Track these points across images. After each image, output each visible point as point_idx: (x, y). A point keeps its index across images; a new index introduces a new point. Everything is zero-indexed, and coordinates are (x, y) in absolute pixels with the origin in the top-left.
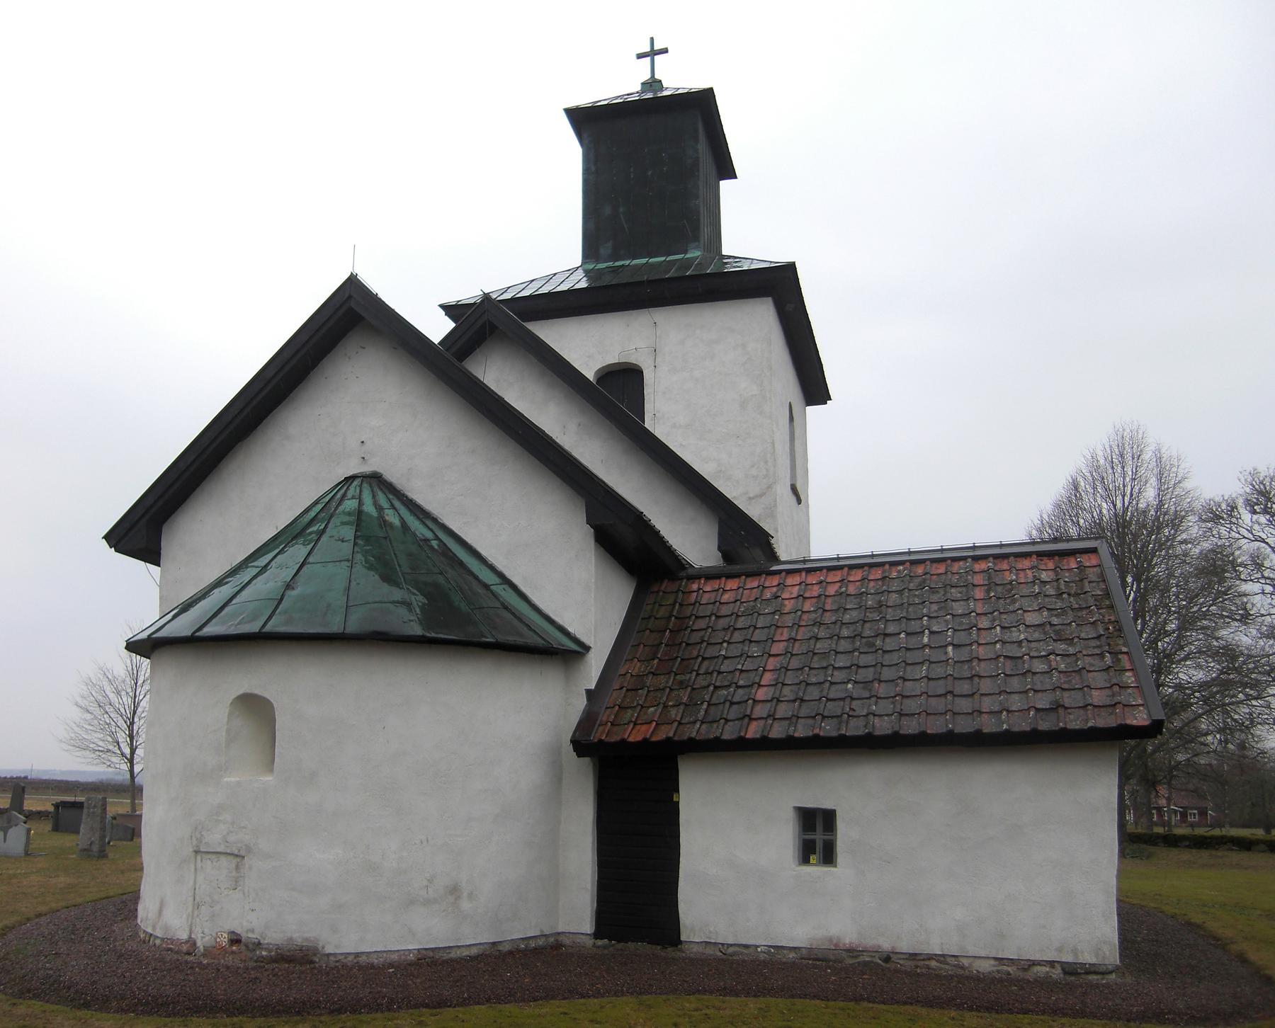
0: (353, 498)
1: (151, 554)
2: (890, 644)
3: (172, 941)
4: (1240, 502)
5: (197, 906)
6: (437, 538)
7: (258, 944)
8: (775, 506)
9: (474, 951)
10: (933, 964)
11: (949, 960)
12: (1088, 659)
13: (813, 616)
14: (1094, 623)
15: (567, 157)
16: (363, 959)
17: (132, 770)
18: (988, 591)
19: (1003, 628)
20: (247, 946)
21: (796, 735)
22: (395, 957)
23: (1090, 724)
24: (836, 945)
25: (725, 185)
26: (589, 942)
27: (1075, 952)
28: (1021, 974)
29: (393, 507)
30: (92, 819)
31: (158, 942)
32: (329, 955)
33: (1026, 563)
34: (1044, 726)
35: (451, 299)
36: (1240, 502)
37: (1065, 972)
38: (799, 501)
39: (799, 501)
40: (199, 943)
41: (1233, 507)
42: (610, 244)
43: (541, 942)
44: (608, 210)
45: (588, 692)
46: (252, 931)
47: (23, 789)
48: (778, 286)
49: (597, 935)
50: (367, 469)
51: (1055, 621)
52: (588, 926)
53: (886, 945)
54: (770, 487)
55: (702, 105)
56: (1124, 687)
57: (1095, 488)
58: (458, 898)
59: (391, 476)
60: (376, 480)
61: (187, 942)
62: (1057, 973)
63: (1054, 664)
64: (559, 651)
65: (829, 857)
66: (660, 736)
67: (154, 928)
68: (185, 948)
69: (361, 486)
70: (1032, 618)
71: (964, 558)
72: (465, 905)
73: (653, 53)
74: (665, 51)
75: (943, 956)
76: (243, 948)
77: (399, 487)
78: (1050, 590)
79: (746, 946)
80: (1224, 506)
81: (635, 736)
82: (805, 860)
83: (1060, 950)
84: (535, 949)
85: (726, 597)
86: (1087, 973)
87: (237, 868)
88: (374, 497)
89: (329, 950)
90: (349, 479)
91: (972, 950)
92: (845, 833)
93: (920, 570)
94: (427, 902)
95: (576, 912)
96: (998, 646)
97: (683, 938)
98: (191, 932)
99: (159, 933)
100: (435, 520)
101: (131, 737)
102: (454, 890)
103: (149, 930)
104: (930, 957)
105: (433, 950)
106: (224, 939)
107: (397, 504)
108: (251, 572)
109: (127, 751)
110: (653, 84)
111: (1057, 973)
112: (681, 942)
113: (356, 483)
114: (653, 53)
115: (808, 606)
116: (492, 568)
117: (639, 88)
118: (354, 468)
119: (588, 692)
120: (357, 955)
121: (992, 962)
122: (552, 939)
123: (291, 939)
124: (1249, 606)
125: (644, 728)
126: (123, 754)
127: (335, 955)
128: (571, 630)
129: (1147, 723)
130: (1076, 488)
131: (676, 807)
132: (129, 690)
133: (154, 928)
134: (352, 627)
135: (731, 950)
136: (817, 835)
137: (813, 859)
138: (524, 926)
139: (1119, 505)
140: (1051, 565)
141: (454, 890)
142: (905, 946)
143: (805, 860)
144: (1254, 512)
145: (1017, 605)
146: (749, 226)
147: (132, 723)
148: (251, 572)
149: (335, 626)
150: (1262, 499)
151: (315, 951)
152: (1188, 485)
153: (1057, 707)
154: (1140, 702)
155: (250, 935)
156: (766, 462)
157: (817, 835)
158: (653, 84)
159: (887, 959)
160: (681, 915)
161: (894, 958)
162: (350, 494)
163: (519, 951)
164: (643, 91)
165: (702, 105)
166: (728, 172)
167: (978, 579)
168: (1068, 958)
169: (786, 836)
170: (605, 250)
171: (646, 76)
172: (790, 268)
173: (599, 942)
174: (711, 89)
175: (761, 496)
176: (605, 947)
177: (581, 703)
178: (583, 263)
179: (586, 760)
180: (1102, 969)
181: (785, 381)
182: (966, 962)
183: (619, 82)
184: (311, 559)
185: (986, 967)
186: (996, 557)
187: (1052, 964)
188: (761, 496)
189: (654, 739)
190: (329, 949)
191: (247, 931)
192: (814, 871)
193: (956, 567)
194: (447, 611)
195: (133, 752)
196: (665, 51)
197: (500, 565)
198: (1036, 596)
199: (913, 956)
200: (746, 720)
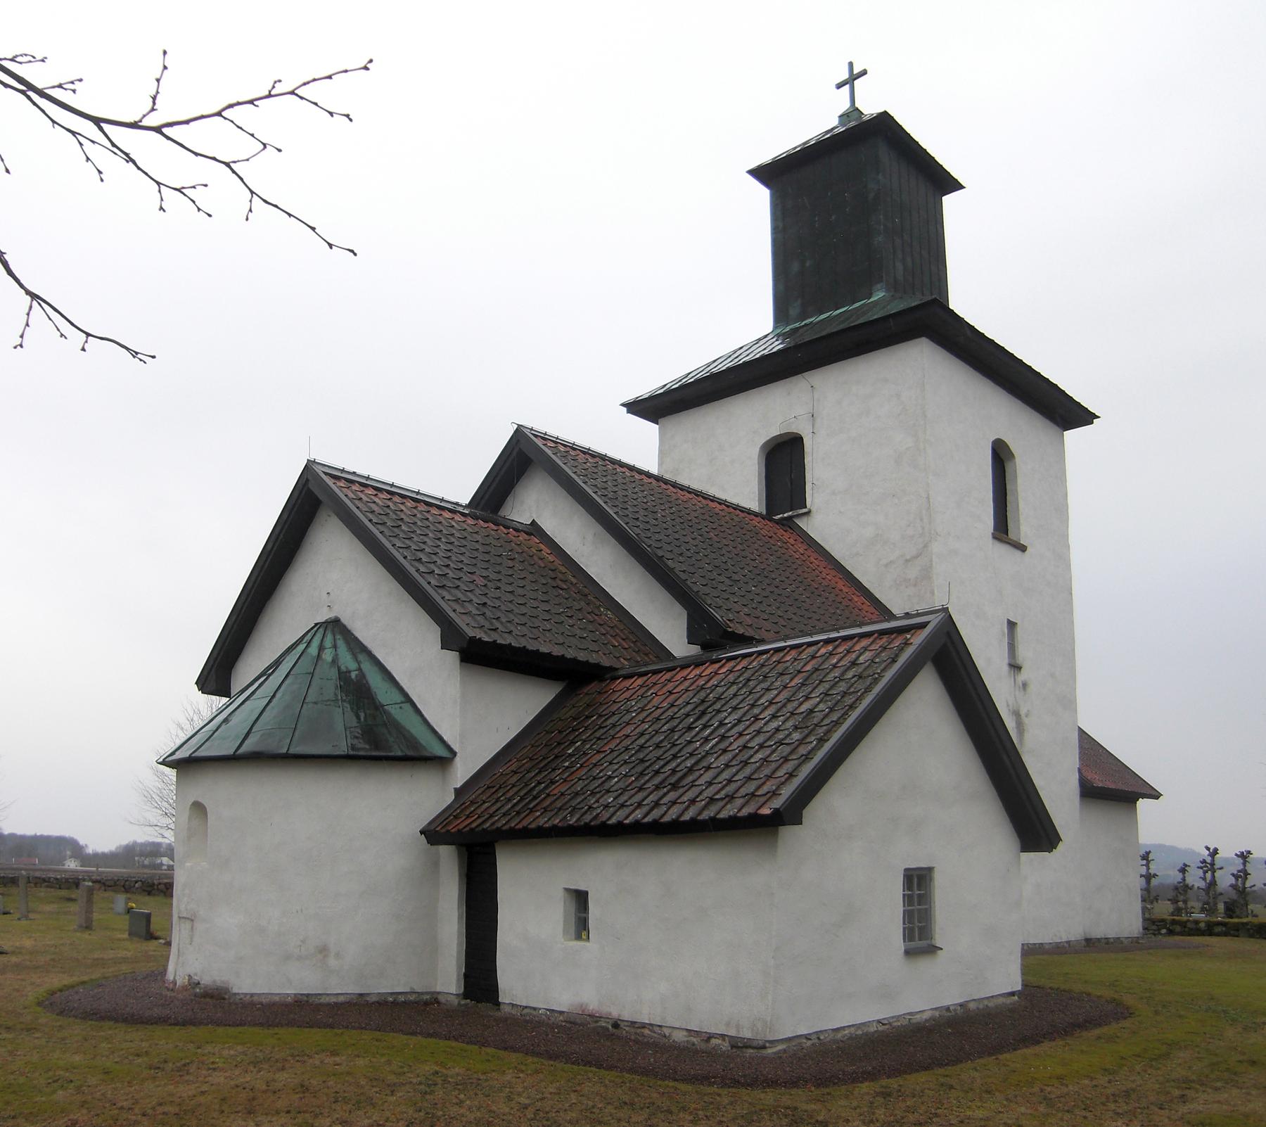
2: (817, 717)
8: (931, 567)
9: (341, 999)
10: (646, 1032)
11: (657, 1029)
16: (255, 998)
22: (277, 999)
25: (948, 201)
27: (738, 1027)
28: (703, 1046)
30: (138, 887)
35: (631, 396)
37: (733, 1047)
42: (799, 302)
44: (795, 267)
47: (1153, 922)
49: (466, 995)
53: (615, 1012)
54: (926, 546)
58: (325, 956)
62: (725, 1046)
72: (332, 962)
73: (854, 78)
79: (535, 1009)
83: (728, 1024)
84: (404, 1002)
86: (747, 1047)
91: (670, 1021)
94: (299, 958)
102: (323, 950)
104: (643, 1026)
105: (308, 995)
108: (256, 685)
111: (725, 1046)
114: (854, 78)
120: (252, 995)
121: (685, 1033)
135: (526, 1011)
138: (396, 980)
141: (323, 950)
148: (256, 685)
151: (227, 990)
156: (921, 520)
158: (853, 111)
159: (616, 1025)
163: (386, 1002)
164: (841, 123)
168: (732, 1033)
170: (794, 311)
171: (845, 106)
173: (463, 1002)
175: (916, 557)
176: (466, 1005)
178: (775, 327)
180: (755, 1044)
182: (667, 1032)
183: (816, 118)
185: (679, 1037)
187: (723, 1036)
188: (916, 557)
189: (610, 822)
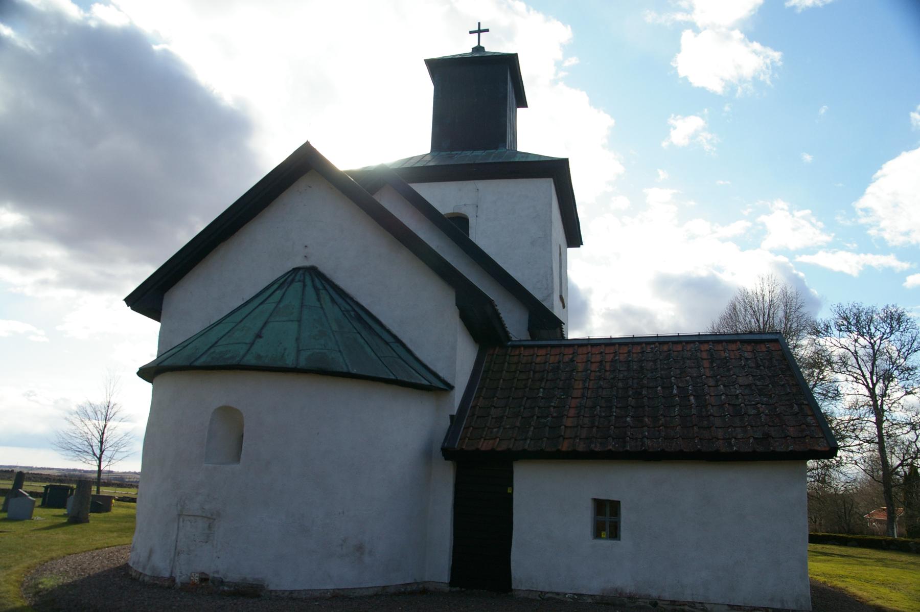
0: (299, 281)
1: (153, 312)
3: (158, 578)
4: (832, 324)
5: (178, 553)
6: (354, 310)
7: (222, 582)
10: (687, 608)
12: (783, 408)
13: (598, 374)
14: (783, 385)
15: (425, 90)
17: (99, 466)
18: (711, 363)
19: (724, 386)
20: (213, 582)
21: (597, 450)
23: (791, 448)
24: (620, 594)
25: (520, 111)
26: (447, 589)
29: (325, 288)
31: (147, 579)
32: (271, 591)
33: (733, 347)
34: (760, 449)
36: (832, 324)
38: (564, 307)
39: (564, 307)
40: (178, 580)
41: (827, 327)
43: (414, 588)
45: (452, 417)
46: (217, 572)
48: (556, 171)
49: (452, 583)
50: (307, 264)
51: (758, 383)
52: (446, 578)
53: (654, 594)
55: (509, 63)
56: (809, 425)
57: (746, 310)
59: (326, 268)
60: (313, 272)
61: (168, 579)
63: (761, 410)
64: (438, 387)
65: (615, 534)
66: (503, 447)
67: (144, 568)
68: (166, 584)
69: (304, 274)
70: (741, 380)
71: (694, 342)
73: (479, 31)
74: (487, 30)
75: (692, 602)
76: (211, 584)
77: (328, 276)
78: (751, 364)
79: (558, 594)
80: (822, 325)
81: (484, 446)
82: (597, 535)
85: (538, 360)
87: (210, 527)
88: (313, 281)
89: (272, 587)
90: (296, 270)
92: (626, 517)
93: (665, 348)
95: (438, 567)
96: (723, 397)
97: (513, 587)
98: (172, 572)
99: (148, 572)
100: (352, 299)
101: (102, 442)
102: (360, 548)
103: (140, 570)
104: (684, 604)
105: (343, 590)
106: (196, 579)
107: (328, 287)
109: (98, 452)
110: (479, 49)
112: (511, 590)
113: (301, 272)
114: (479, 31)
115: (594, 367)
116: (389, 332)
117: (470, 51)
118: (299, 262)
119: (452, 417)
122: (421, 586)
123: (245, 578)
124: (840, 388)
125: (491, 442)
126: (94, 454)
127: (276, 591)
128: (441, 375)
129: (827, 449)
130: (735, 309)
131: (510, 498)
132: (103, 411)
133: (144, 568)
134: (302, 363)
135: (548, 595)
136: (607, 518)
137: (603, 535)
139: (761, 320)
140: (749, 348)
141: (360, 548)
142: (668, 595)
143: (597, 535)
144: (841, 330)
145: (732, 372)
146: (533, 134)
147: (103, 433)
149: (290, 362)
150: (845, 323)
152: (802, 310)
153: (767, 436)
154: (821, 435)
155: (216, 575)
157: (607, 518)
158: (479, 49)
160: (513, 572)
161: (660, 603)
162: (297, 278)
165: (509, 63)
166: (522, 103)
167: (705, 355)
169: (586, 518)
172: (565, 162)
173: (454, 589)
174: (516, 55)
177: (446, 423)
179: (449, 463)
181: (558, 232)
184: (234, 325)
186: (714, 342)
190: (272, 587)
191: (214, 572)
192: (605, 543)
193: (689, 347)
194: (371, 357)
195: (102, 452)
196: (487, 30)
197: (395, 330)
198: (743, 367)
199: (673, 603)
200: (561, 439)
